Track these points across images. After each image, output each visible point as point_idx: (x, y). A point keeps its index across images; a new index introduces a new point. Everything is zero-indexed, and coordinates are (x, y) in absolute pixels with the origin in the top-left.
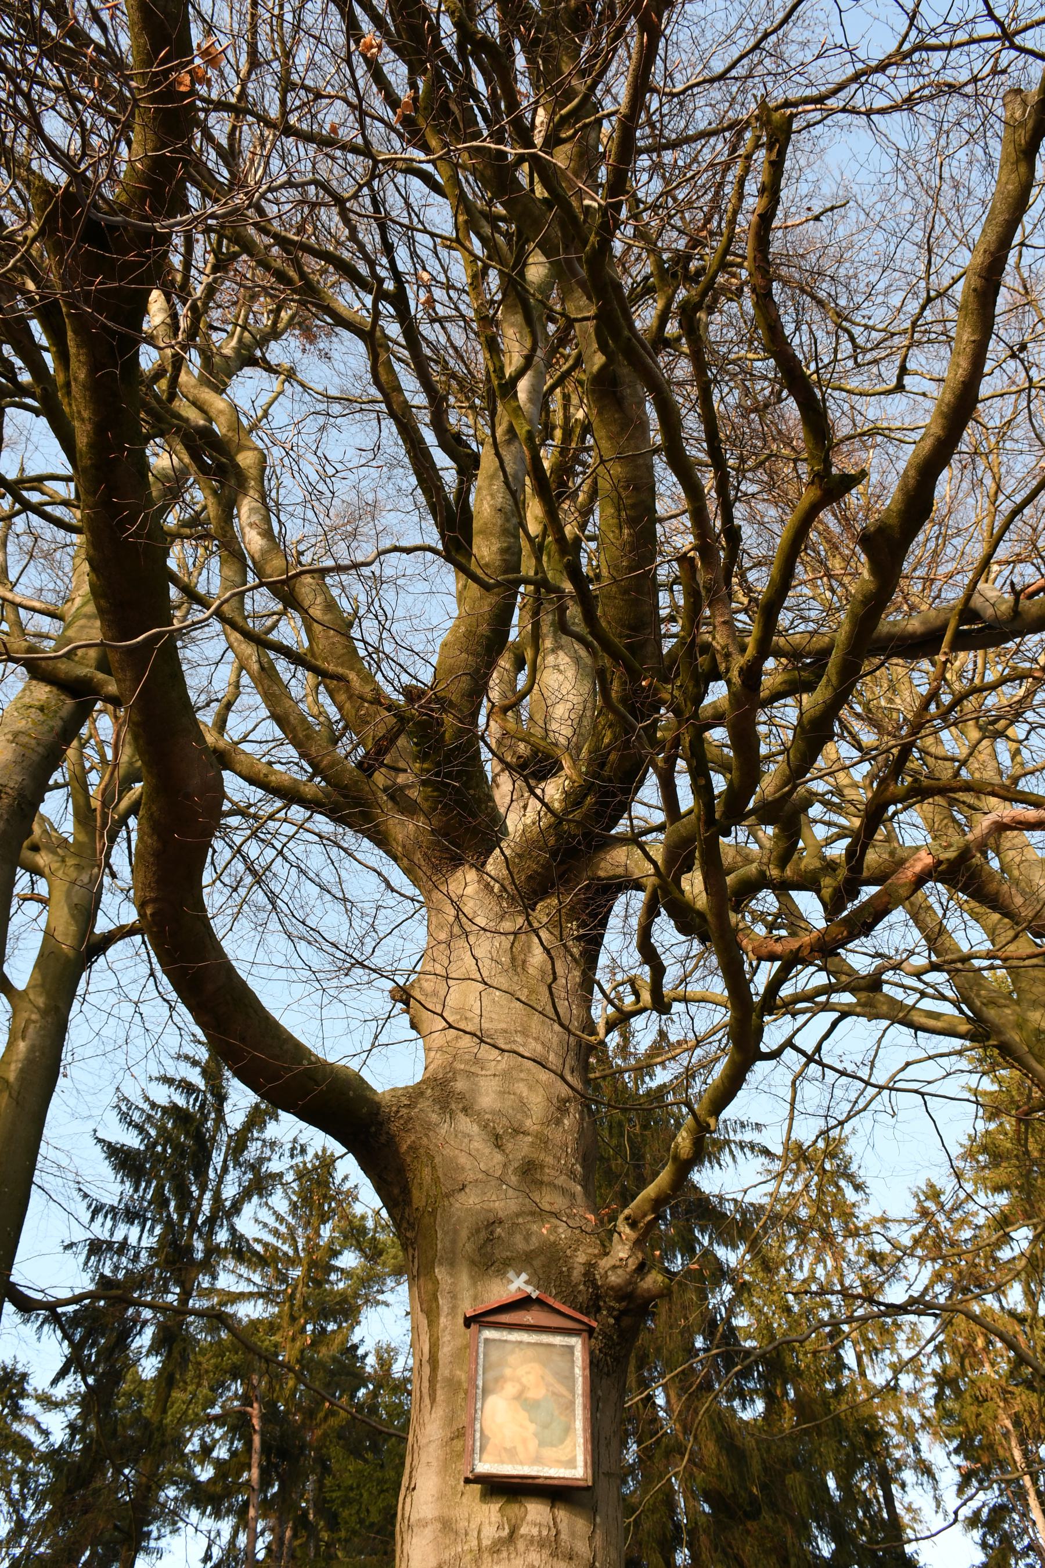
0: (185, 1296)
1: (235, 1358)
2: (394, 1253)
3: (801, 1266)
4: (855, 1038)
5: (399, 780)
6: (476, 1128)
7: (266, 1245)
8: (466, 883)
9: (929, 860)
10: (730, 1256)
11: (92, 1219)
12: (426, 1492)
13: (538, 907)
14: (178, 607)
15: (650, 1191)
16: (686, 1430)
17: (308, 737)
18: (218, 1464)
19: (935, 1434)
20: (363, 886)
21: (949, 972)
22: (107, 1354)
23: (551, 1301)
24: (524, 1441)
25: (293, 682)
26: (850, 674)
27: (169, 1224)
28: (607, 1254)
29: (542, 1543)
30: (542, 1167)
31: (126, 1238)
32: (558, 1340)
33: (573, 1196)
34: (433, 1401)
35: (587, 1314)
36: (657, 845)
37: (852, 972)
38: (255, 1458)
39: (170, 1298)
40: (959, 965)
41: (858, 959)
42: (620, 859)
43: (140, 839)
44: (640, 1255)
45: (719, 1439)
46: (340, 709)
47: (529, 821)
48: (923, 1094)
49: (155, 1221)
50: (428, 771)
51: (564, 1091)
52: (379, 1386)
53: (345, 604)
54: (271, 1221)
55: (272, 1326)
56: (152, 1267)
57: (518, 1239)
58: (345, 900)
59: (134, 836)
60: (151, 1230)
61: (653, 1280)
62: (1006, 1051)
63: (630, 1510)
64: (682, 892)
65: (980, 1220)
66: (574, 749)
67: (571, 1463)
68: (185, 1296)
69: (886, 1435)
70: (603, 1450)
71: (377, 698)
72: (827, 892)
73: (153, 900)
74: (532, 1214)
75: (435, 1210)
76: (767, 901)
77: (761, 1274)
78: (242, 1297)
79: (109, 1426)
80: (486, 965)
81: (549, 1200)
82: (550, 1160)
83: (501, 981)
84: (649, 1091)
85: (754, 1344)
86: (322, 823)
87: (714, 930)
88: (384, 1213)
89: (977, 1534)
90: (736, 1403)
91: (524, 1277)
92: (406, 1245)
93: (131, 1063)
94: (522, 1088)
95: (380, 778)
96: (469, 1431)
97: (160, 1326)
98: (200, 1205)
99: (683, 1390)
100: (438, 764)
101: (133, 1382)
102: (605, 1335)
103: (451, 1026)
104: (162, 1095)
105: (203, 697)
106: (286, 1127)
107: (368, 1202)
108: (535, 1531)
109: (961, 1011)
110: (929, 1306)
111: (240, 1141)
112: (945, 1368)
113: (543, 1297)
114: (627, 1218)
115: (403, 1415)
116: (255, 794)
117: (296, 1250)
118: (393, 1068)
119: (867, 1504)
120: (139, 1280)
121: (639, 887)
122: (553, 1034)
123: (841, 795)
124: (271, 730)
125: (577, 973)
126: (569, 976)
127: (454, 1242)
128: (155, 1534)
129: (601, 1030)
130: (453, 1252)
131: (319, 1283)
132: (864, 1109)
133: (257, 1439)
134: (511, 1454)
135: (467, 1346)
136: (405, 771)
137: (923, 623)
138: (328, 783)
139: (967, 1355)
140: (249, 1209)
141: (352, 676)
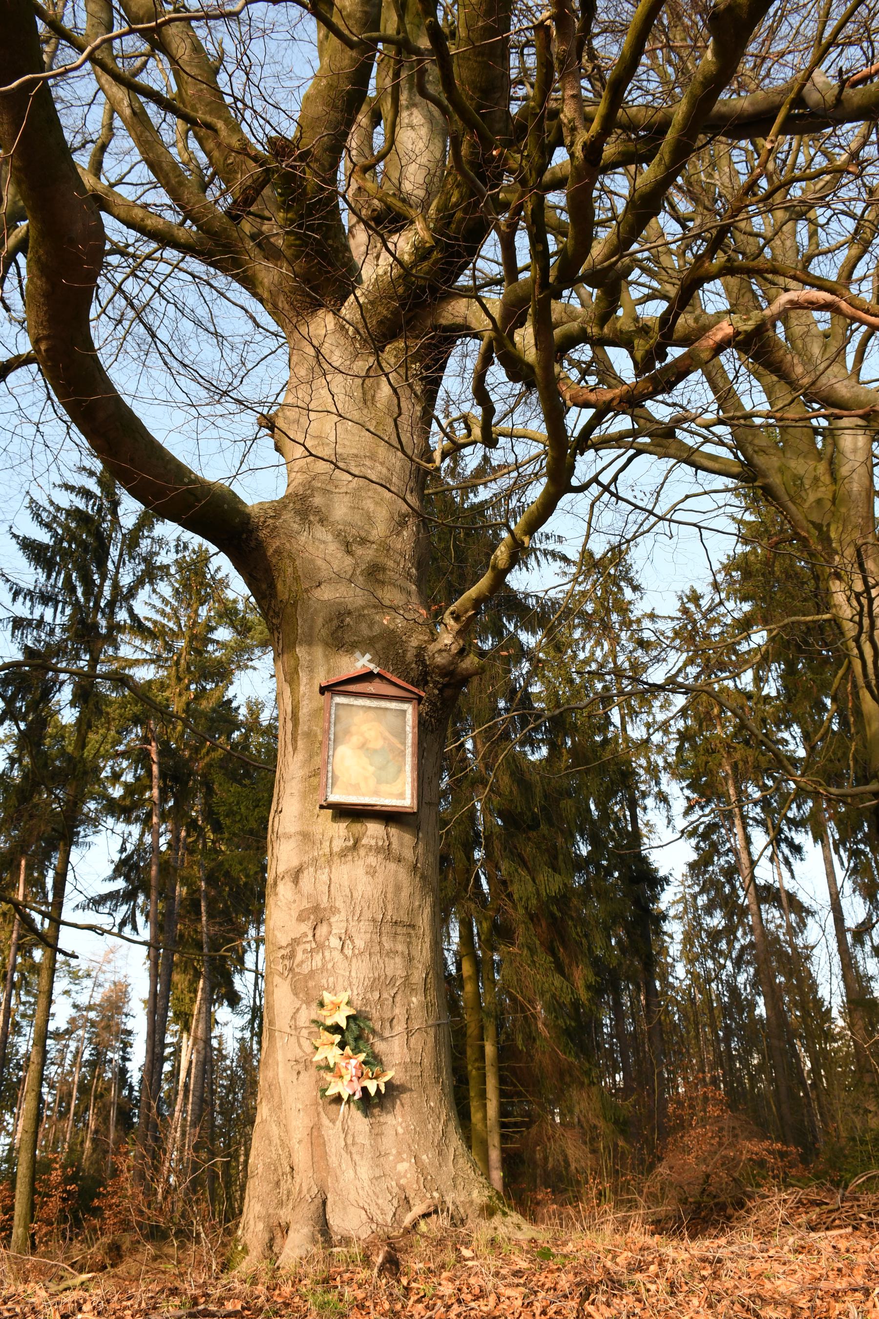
0: (94, 662)
1: (135, 709)
2: (261, 630)
3: (584, 648)
4: (647, 470)
5: (265, 228)
6: (329, 538)
7: (155, 623)
8: (323, 324)
9: (729, 330)
10: (528, 639)
11: (14, 600)
12: (290, 812)
13: (387, 348)
14: (47, 42)
15: (472, 592)
16: (488, 767)
17: (181, 184)
18: (126, 785)
19: (673, 774)
20: (233, 323)
21: (731, 426)
22: (33, 707)
23: (389, 676)
24: (366, 779)
25: (164, 125)
26: (683, 152)
27: (76, 605)
28: (434, 640)
29: (378, 850)
30: (384, 569)
31: (42, 617)
32: (394, 705)
33: (409, 593)
34: (295, 749)
35: (417, 687)
36: (494, 298)
37: (651, 419)
38: (155, 781)
39: (82, 663)
40: (742, 421)
41: (659, 410)
42: (459, 309)
43: (30, 280)
44: (461, 642)
45: (512, 774)
46: (208, 154)
47: (381, 271)
48: (700, 528)
49: (65, 603)
50: (292, 221)
51: (405, 508)
52: (250, 730)
53: (209, 47)
54: (159, 604)
55: (163, 686)
56: (66, 640)
57: (364, 626)
58: (216, 334)
59: (24, 272)
60: (63, 612)
61: (471, 662)
62: (768, 492)
63: (444, 823)
64: (514, 345)
65: (729, 620)
66: (425, 205)
67: (402, 796)
68: (94, 662)
69: (638, 774)
70: (426, 786)
71: (245, 149)
72: (639, 354)
73: (46, 338)
74: (375, 607)
75: (296, 602)
76: (584, 353)
77: (552, 653)
78: (137, 663)
79: (41, 759)
80: (340, 398)
81: (390, 595)
82: (390, 564)
83: (356, 415)
84: (473, 507)
85: (543, 705)
86: (196, 265)
87: (540, 381)
88: (252, 599)
89: (693, 842)
90: (527, 748)
91: (368, 656)
92: (267, 613)
93: (36, 475)
94: (369, 505)
95: (247, 226)
96: (323, 772)
97: (76, 684)
98: (101, 592)
99: (488, 738)
100: (301, 217)
101: (56, 727)
102: (431, 702)
103: (311, 455)
104: (65, 499)
105: (79, 138)
106: (168, 530)
107: (238, 589)
108: (373, 842)
109: (736, 457)
110: (681, 685)
111: (132, 540)
112: (687, 728)
113: (383, 672)
114: (452, 613)
115: (272, 755)
116: (132, 235)
117: (180, 626)
118: (261, 483)
119: (617, 820)
120: (58, 650)
121: (476, 336)
122: (396, 460)
123: (657, 262)
124: (143, 173)
125: (418, 408)
126: (411, 409)
127: (311, 628)
128: (82, 834)
129: (437, 456)
130: (311, 636)
131: (199, 653)
132: (648, 531)
133: (155, 769)
134: (356, 788)
135: (321, 709)
136: (270, 219)
137: (751, 104)
138: (199, 228)
139: (705, 720)
140: (144, 593)
141: (220, 125)
